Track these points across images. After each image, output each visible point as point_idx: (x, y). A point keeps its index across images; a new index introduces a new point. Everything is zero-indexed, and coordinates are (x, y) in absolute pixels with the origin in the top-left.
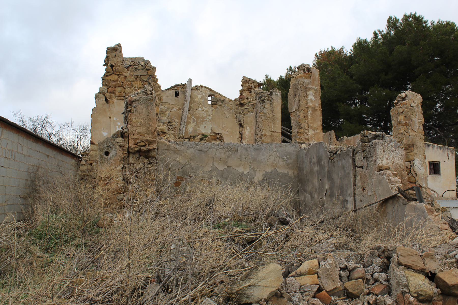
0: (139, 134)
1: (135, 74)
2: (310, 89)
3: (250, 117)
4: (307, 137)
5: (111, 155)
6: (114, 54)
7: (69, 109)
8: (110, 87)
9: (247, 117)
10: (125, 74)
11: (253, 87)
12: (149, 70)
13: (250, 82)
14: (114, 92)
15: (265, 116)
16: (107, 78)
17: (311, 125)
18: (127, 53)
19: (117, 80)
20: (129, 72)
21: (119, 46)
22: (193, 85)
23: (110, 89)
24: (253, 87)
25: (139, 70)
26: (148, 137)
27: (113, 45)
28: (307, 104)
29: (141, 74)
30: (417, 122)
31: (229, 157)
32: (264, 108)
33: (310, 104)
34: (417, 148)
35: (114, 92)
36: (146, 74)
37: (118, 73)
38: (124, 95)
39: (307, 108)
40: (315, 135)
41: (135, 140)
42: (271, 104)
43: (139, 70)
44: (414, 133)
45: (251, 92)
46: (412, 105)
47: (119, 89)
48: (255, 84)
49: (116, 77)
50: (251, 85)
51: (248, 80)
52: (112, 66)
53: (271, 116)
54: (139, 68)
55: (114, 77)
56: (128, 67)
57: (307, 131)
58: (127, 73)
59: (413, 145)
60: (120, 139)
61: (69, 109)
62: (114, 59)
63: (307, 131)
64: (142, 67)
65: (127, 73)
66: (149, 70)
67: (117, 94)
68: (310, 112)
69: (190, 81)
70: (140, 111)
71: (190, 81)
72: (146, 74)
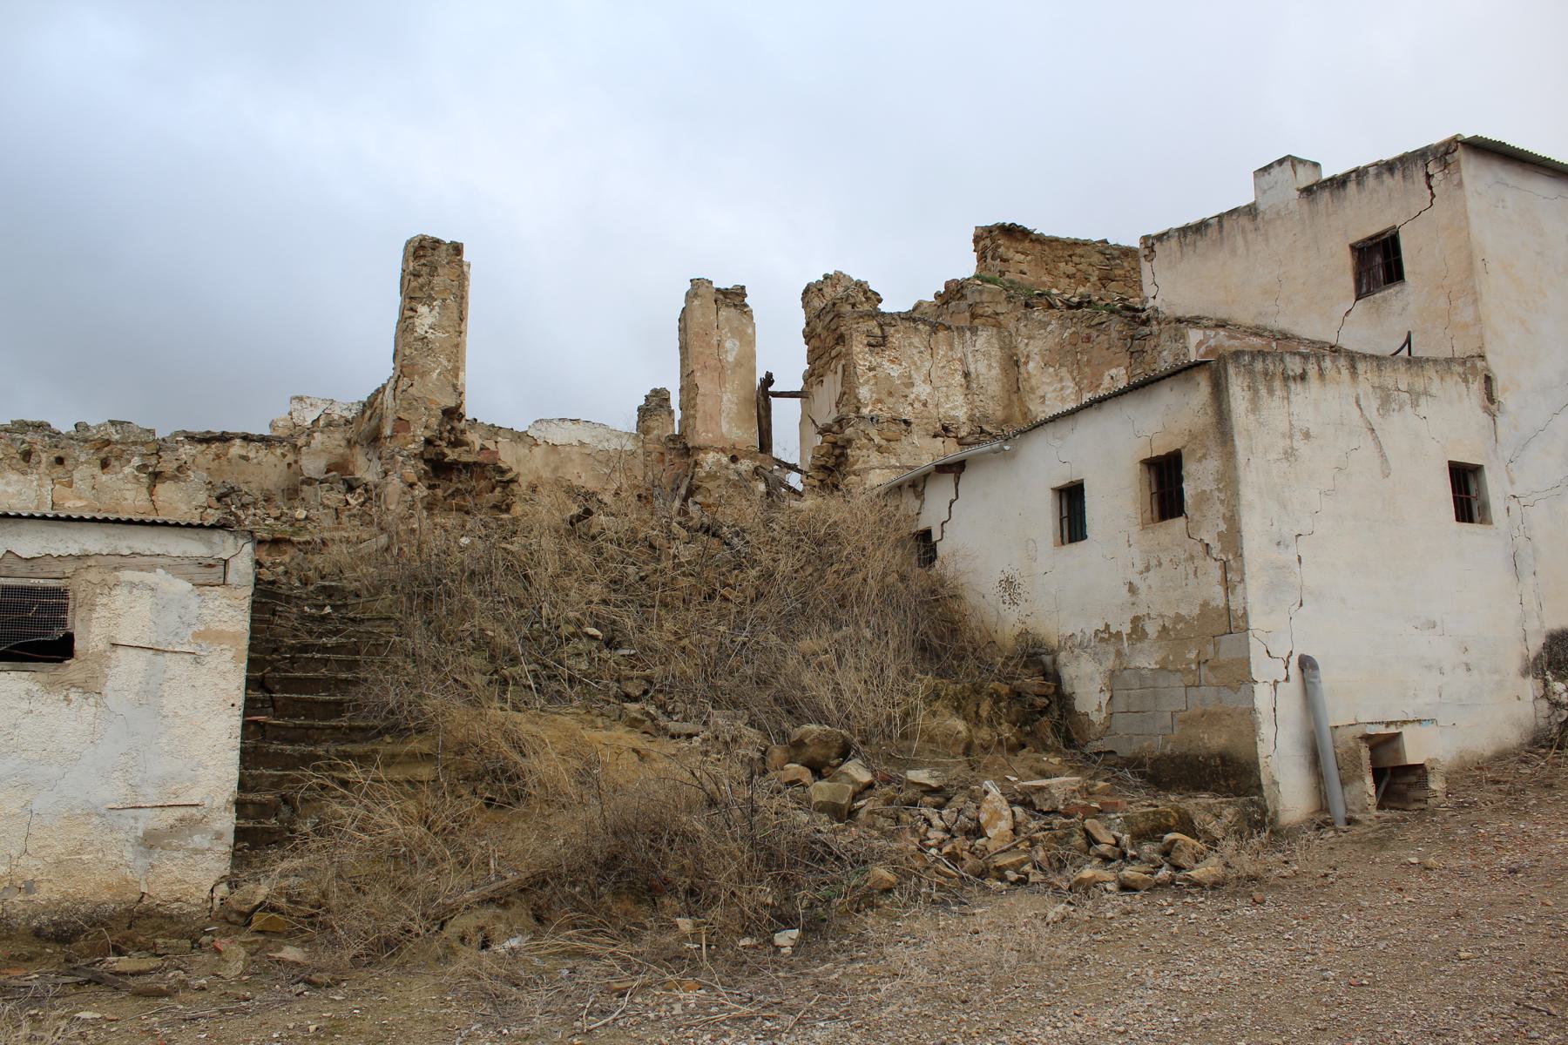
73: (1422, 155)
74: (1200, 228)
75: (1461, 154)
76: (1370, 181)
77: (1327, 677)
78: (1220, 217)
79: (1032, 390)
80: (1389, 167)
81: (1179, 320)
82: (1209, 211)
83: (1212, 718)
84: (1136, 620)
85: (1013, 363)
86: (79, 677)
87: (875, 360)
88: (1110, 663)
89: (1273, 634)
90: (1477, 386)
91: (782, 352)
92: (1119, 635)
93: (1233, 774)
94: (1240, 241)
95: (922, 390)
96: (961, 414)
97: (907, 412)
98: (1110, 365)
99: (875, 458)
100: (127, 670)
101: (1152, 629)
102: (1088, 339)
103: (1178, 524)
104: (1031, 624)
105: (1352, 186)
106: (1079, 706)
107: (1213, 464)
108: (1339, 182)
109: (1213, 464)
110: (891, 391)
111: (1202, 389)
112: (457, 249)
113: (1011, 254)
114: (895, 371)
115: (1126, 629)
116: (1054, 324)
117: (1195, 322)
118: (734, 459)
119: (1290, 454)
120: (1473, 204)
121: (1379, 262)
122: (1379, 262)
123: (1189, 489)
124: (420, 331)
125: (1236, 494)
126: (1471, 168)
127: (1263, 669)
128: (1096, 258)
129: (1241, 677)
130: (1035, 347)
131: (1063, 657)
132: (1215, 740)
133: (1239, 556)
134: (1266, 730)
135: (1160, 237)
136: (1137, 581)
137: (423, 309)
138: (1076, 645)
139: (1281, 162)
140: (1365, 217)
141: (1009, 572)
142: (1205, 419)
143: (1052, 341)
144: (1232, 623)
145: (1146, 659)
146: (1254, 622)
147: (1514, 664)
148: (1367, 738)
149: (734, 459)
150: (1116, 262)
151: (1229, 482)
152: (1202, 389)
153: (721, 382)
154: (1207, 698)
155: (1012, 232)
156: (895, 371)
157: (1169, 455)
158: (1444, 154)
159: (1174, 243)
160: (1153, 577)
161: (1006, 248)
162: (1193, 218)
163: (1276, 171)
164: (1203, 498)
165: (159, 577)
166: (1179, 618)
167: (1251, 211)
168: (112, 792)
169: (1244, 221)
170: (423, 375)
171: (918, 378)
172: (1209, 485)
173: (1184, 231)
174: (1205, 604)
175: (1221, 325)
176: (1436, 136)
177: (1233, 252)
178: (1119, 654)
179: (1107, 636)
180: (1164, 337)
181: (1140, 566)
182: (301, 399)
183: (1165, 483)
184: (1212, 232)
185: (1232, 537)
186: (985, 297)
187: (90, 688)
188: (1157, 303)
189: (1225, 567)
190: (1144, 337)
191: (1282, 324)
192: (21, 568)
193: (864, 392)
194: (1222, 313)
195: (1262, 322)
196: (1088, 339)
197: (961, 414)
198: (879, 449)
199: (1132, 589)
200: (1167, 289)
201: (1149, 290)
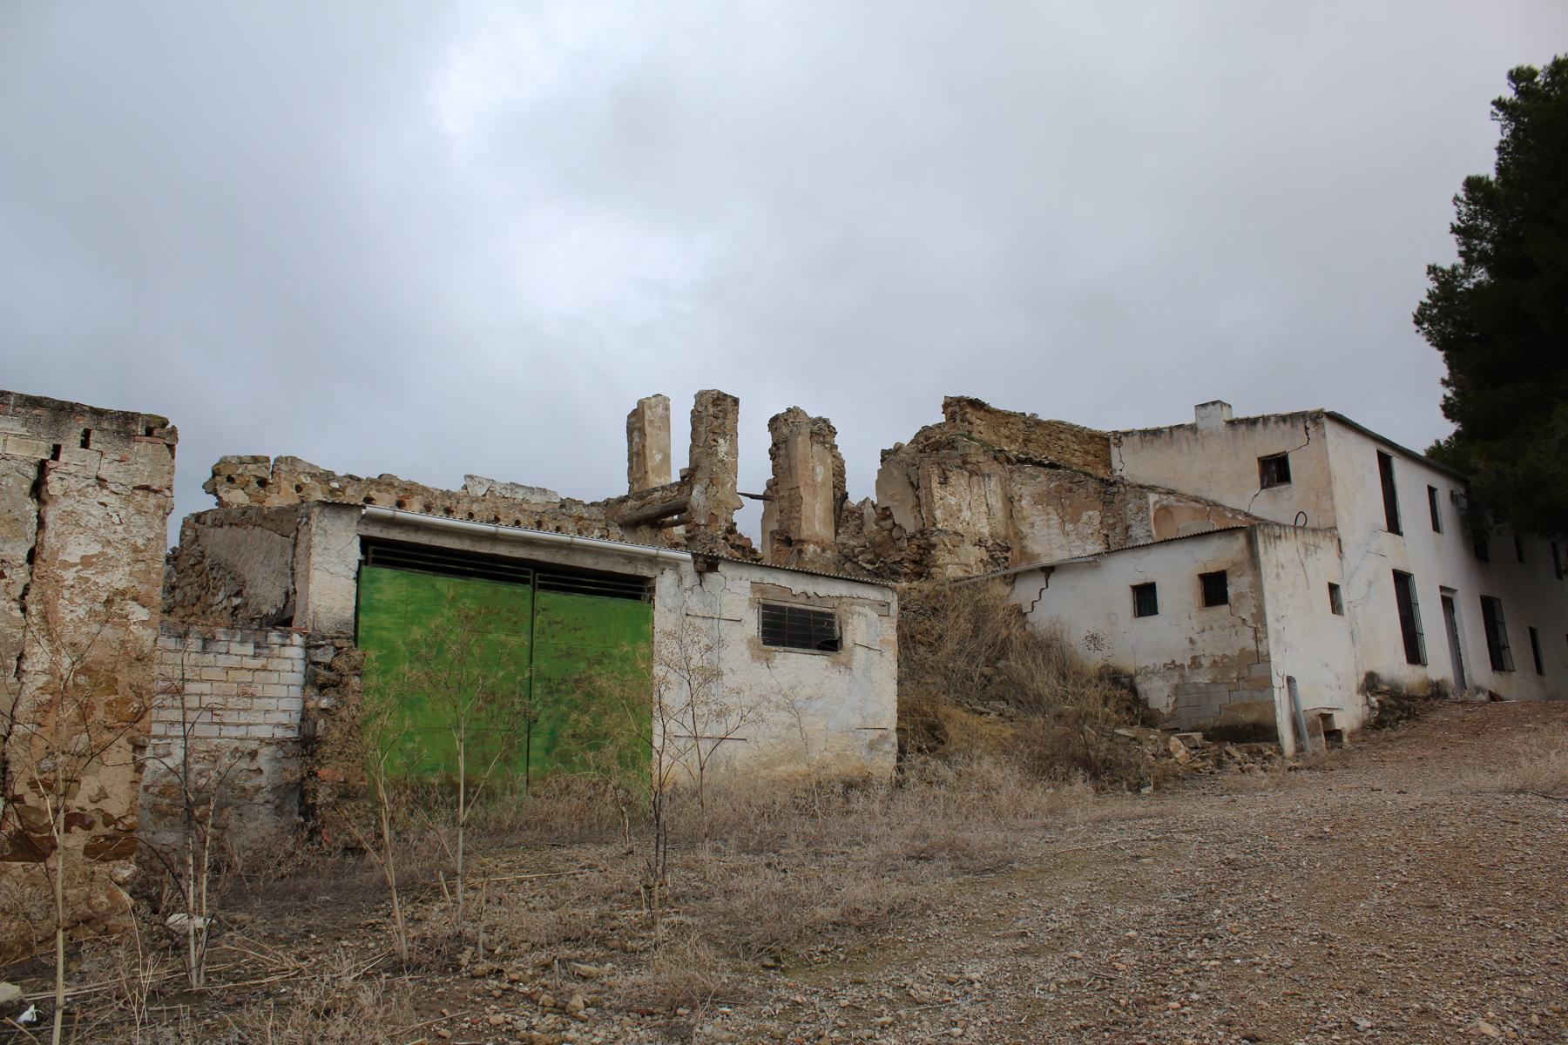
71: (1457, 199)
73: (1303, 416)
74: (1157, 433)
75: (1325, 419)
76: (1271, 425)
77: (1300, 687)
78: (1171, 428)
79: (1024, 518)
80: (1284, 419)
81: (1141, 487)
82: (1164, 423)
83: (1247, 707)
84: (1194, 658)
85: (1009, 500)
86: (844, 659)
87: (943, 493)
88: (1176, 680)
89: (1281, 666)
90: (1335, 543)
91: (753, 464)
92: (1182, 666)
93: (1264, 732)
94: (1184, 445)
95: (966, 514)
96: (986, 531)
97: (959, 528)
98: (1088, 508)
99: (948, 558)
100: (860, 653)
101: (1206, 662)
102: (1071, 490)
103: (1225, 609)
104: (1112, 661)
105: (1260, 425)
106: (1152, 705)
107: (1247, 579)
108: (1251, 422)
109: (1247, 579)
110: (953, 514)
111: (1241, 541)
112: (736, 401)
113: (973, 419)
114: (953, 501)
115: (1187, 662)
116: (1042, 478)
117: (1152, 488)
118: (823, 550)
119: (1278, 575)
120: (1331, 447)
121: (1275, 470)
122: (1275, 470)
123: (1231, 591)
124: (721, 455)
125: (1262, 595)
126: (1330, 428)
127: (1278, 682)
128: (1022, 426)
129: (1266, 684)
130: (1025, 491)
131: (1138, 679)
132: (1251, 717)
133: (1265, 625)
134: (1278, 711)
135: (1126, 434)
136: (1195, 637)
137: (721, 441)
138: (1151, 673)
139: (1214, 403)
140: (1270, 443)
141: (1092, 631)
142: (1245, 555)
143: (1040, 488)
144: (1262, 659)
145: (1202, 678)
146: (1273, 658)
147: (1354, 688)
148: (1321, 715)
149: (823, 550)
150: (1101, 444)
151: (1257, 588)
152: (1241, 541)
153: (815, 497)
154: (1244, 695)
155: (976, 404)
156: (953, 501)
157: (1396, 581)
158: (1317, 417)
159: (1136, 438)
160: (1206, 635)
161: (971, 414)
162: (1151, 426)
163: (1210, 408)
164: (1240, 596)
165: (866, 610)
166: (1225, 656)
167: (1193, 428)
168: (856, 721)
169: (1188, 433)
170: (723, 485)
171: (964, 506)
172: (1245, 590)
173: (1145, 433)
174: (1242, 650)
175: (1170, 492)
176: (1311, 407)
177: (1180, 450)
178: (1181, 676)
179: (1173, 666)
180: (1128, 496)
181: (1197, 629)
182: (471, 477)
183: (1214, 588)
184: (1165, 437)
185: (1260, 616)
186: (972, 451)
187: (847, 666)
188: (1123, 473)
189: (1256, 631)
190: (1114, 494)
191: (1212, 497)
192: (818, 601)
193: (938, 514)
194: (1172, 486)
195: (1200, 494)
196: (1071, 490)
197: (986, 531)
198: (949, 552)
199: (1192, 641)
200: (1129, 465)
201: (1116, 464)
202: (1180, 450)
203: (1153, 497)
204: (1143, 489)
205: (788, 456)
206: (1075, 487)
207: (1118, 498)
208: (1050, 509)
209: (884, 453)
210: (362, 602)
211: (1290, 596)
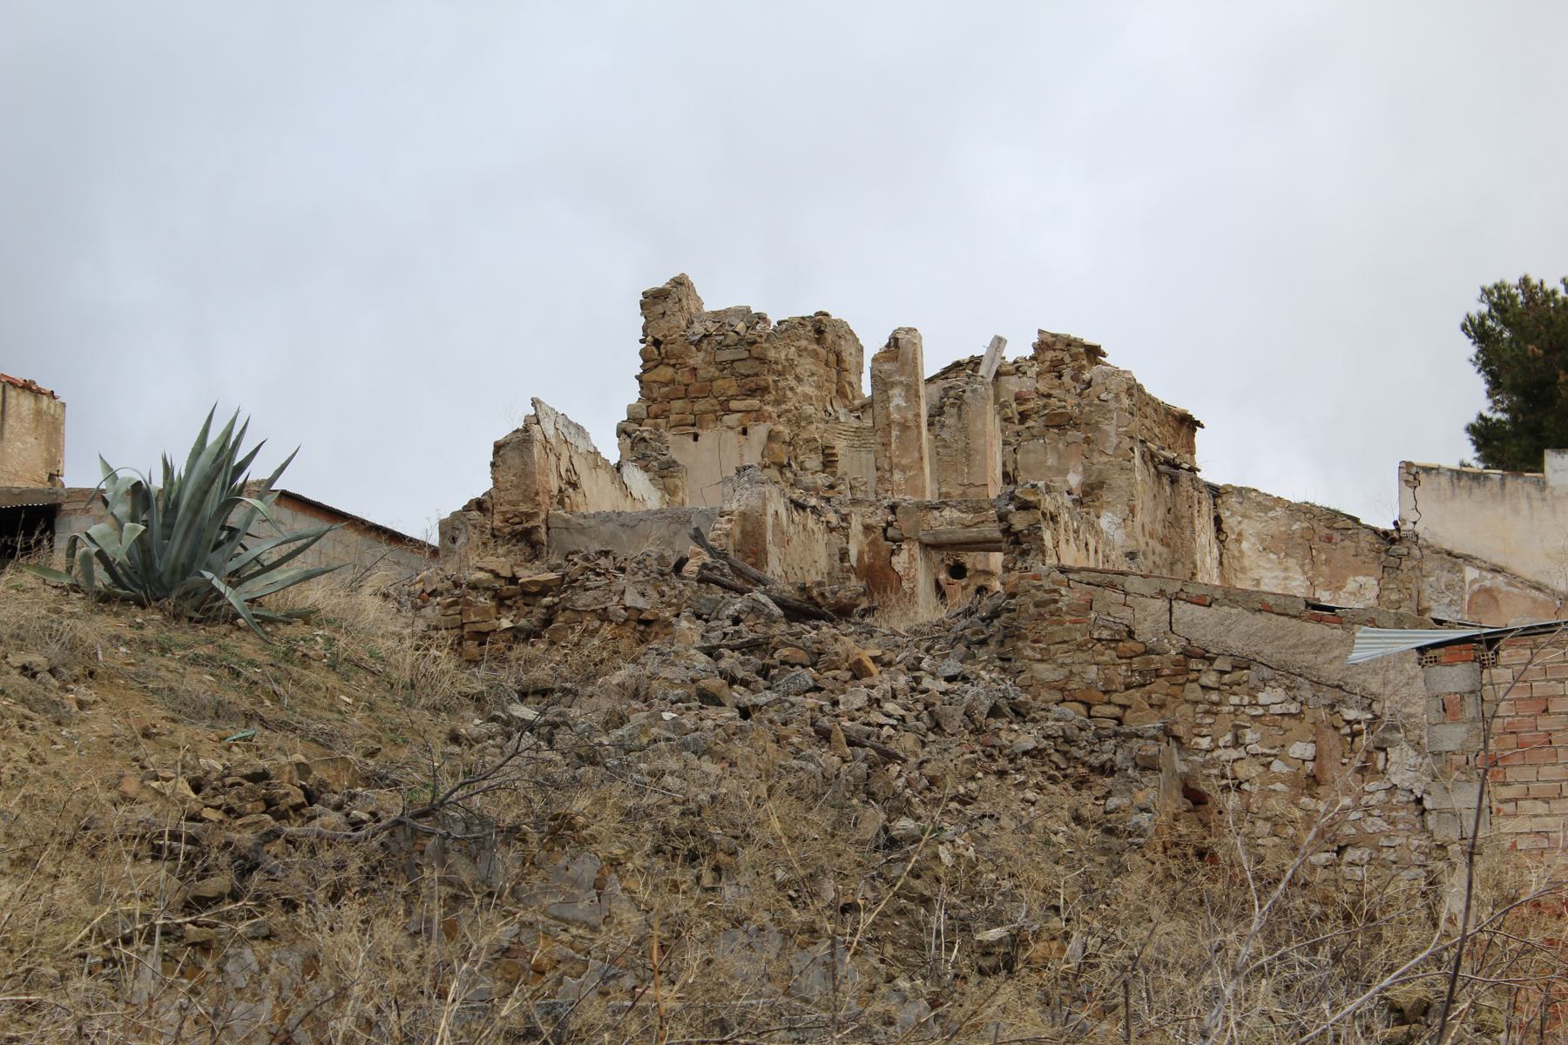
0: (510, 503)
1: (718, 359)
2: (893, 385)
3: (1035, 452)
4: (888, 486)
5: (459, 542)
6: (659, 309)
7: (1552, 459)
8: (654, 400)
9: (1028, 452)
10: (691, 362)
11: (1067, 359)
12: (755, 342)
13: (1059, 346)
14: (664, 414)
15: (945, 447)
16: (646, 377)
17: (895, 460)
18: (715, 296)
19: (673, 381)
20: (701, 355)
21: (680, 282)
22: (931, 365)
23: (655, 408)
24: (1067, 359)
25: (728, 346)
26: (524, 508)
27: (660, 282)
28: (888, 416)
29: (732, 357)
30: (1113, 433)
31: (675, 534)
32: (943, 426)
33: (895, 416)
34: (1111, 489)
35: (664, 414)
36: (746, 355)
37: (673, 361)
38: (691, 419)
39: (889, 425)
40: (906, 481)
41: (504, 513)
42: (960, 416)
43: (728, 346)
44: (1104, 459)
45: (1060, 377)
46: (1103, 396)
47: (677, 405)
48: (1074, 350)
49: (670, 371)
50: (1060, 355)
51: (1051, 340)
52: (657, 343)
53: (961, 445)
54: (728, 342)
55: (665, 373)
56: (700, 341)
57: (888, 475)
58: (697, 359)
59: (1101, 485)
60: (475, 514)
61: (1552, 459)
62: (662, 322)
63: (888, 475)
64: (736, 337)
65: (697, 359)
66: (755, 342)
67: (673, 417)
68: (895, 433)
69: (999, 342)
70: (510, 462)
71: (999, 342)
72: (746, 355)
79: (1243, 570)
94: (1524, 504)
98: (1356, 572)
102: (1329, 539)
117: (1468, 559)
135: (1427, 470)
143: (1273, 528)
159: (1444, 480)
175: (1496, 570)
188: (1419, 528)
190: (1400, 557)
194: (1498, 560)
195: (1544, 580)
196: (1329, 539)
202: (1516, 511)
203: (1470, 573)
204: (1455, 559)
205: (964, 429)
206: (1337, 536)
207: (1407, 564)
208: (1291, 562)
209: (1187, 424)
210: (337, 545)
211: (771, 721)
